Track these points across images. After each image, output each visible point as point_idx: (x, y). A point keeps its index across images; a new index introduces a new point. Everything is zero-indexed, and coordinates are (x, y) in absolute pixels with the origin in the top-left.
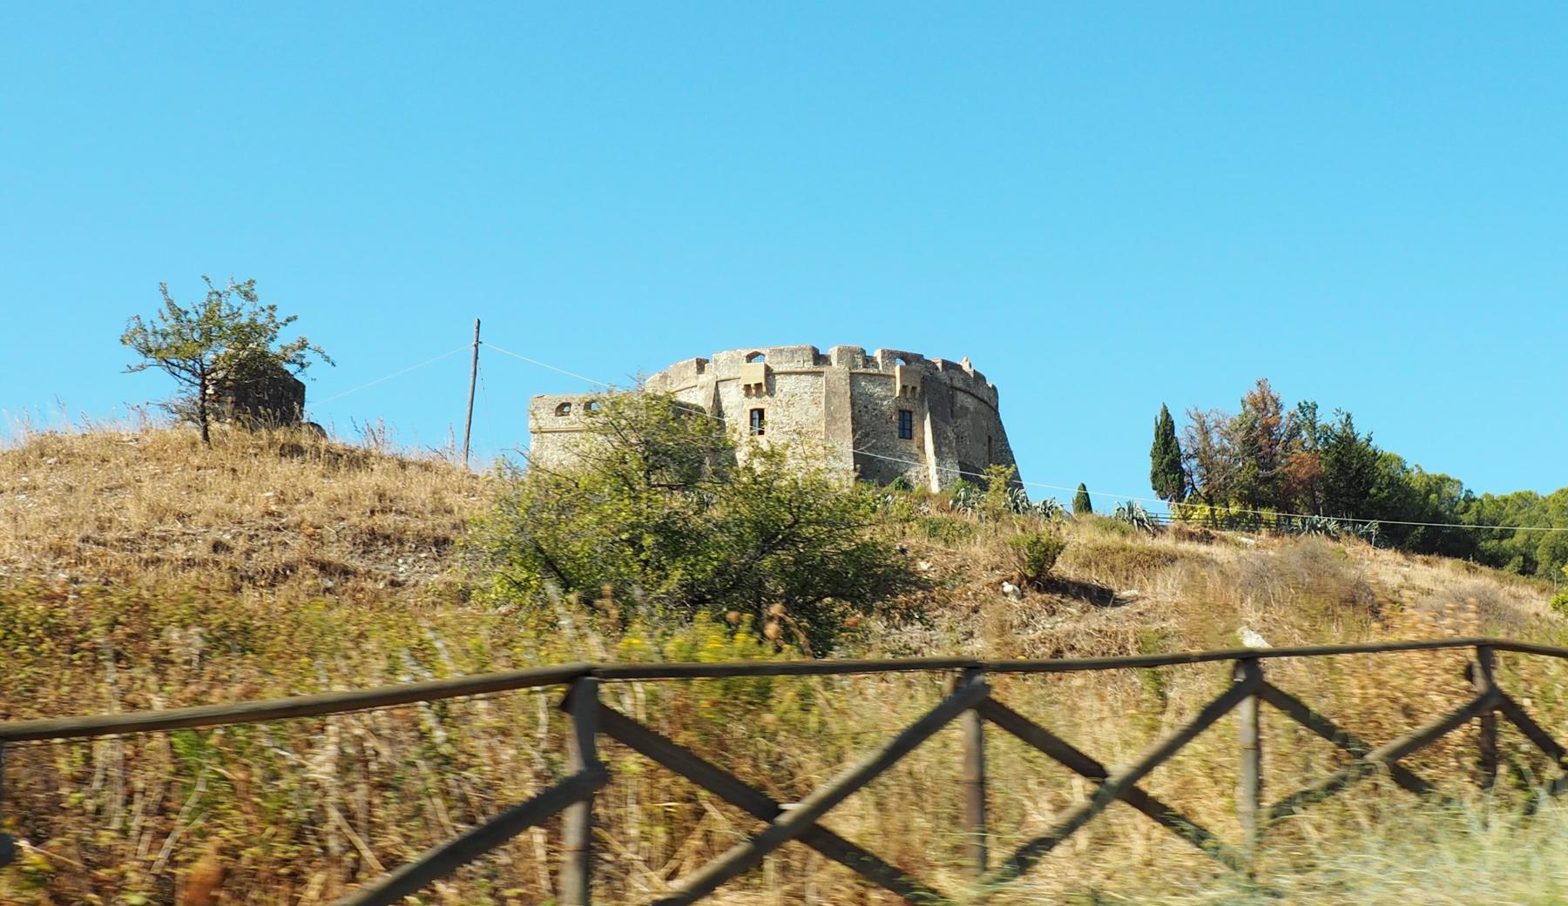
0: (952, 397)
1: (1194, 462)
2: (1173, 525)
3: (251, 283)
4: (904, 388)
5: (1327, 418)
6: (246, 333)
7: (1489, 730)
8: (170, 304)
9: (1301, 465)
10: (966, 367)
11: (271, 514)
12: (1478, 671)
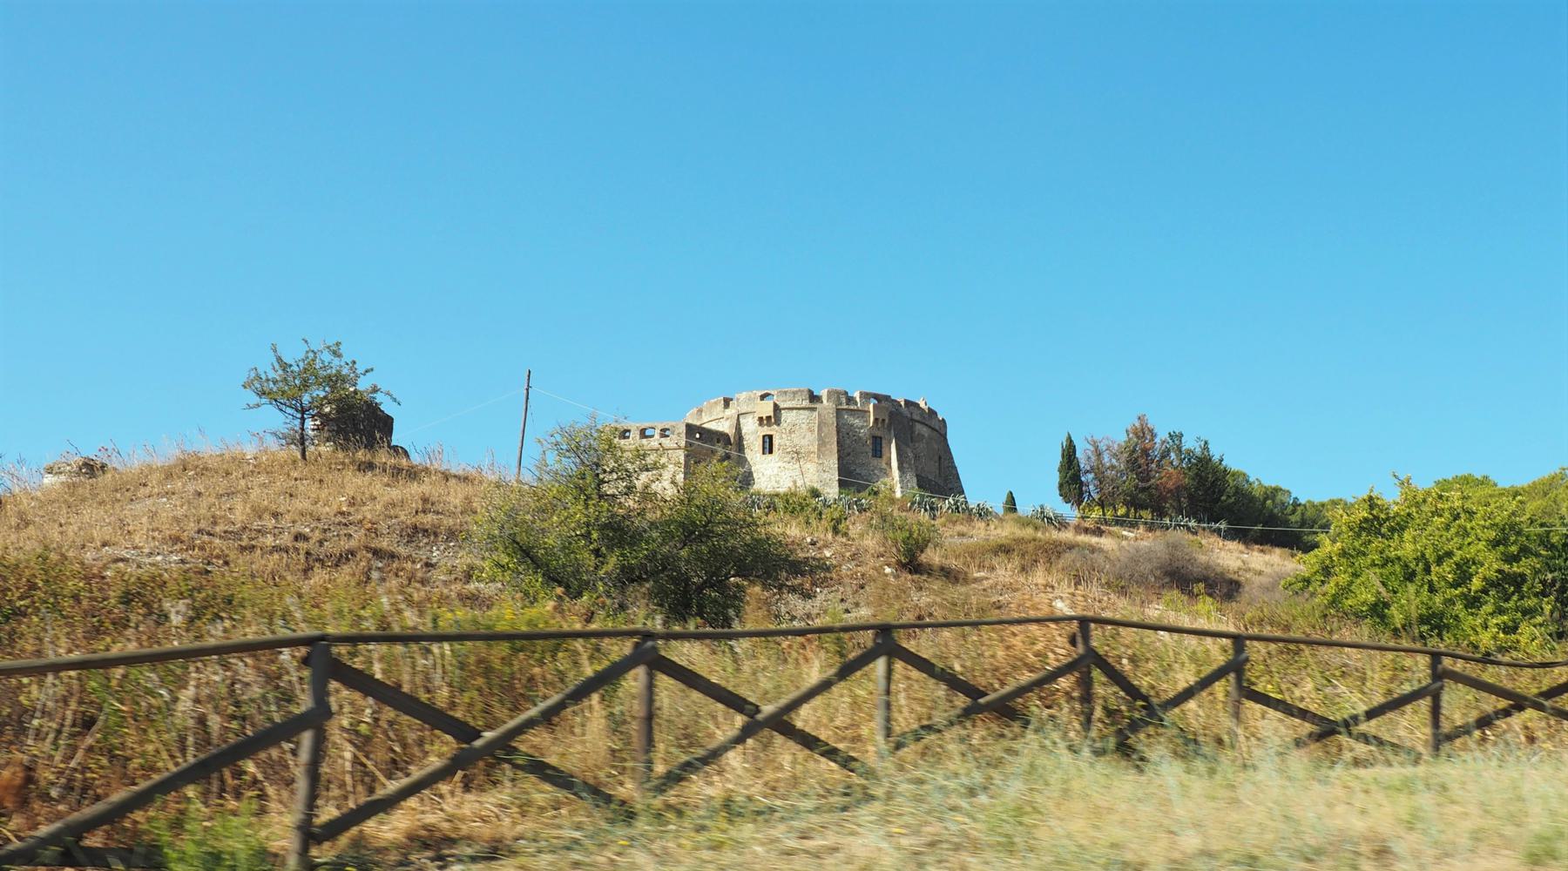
0: (912, 428)
1: (1091, 476)
2: (1075, 521)
3: (338, 344)
4: (876, 420)
5: (1189, 443)
6: (335, 381)
7: (1086, 684)
8: (279, 359)
9: (1170, 478)
10: (922, 405)
11: (342, 513)
12: (1079, 639)
